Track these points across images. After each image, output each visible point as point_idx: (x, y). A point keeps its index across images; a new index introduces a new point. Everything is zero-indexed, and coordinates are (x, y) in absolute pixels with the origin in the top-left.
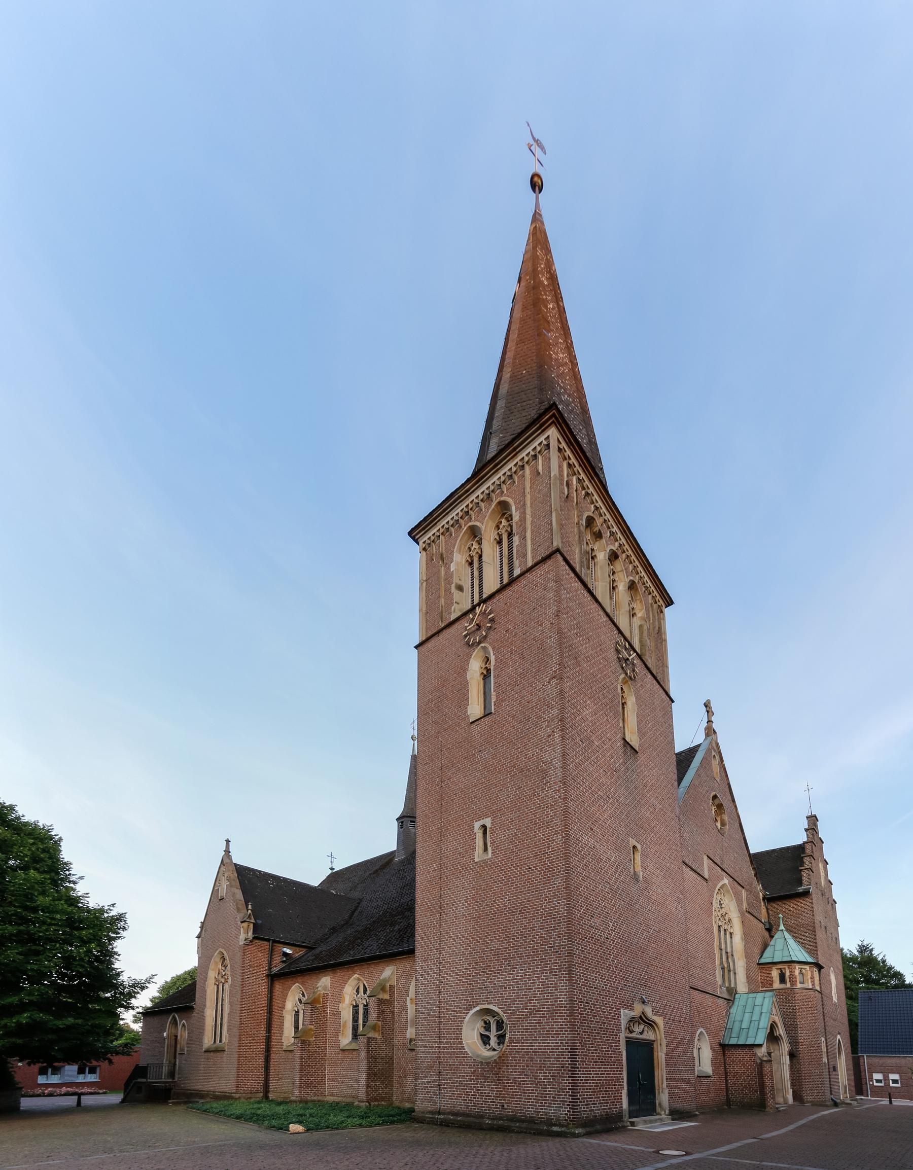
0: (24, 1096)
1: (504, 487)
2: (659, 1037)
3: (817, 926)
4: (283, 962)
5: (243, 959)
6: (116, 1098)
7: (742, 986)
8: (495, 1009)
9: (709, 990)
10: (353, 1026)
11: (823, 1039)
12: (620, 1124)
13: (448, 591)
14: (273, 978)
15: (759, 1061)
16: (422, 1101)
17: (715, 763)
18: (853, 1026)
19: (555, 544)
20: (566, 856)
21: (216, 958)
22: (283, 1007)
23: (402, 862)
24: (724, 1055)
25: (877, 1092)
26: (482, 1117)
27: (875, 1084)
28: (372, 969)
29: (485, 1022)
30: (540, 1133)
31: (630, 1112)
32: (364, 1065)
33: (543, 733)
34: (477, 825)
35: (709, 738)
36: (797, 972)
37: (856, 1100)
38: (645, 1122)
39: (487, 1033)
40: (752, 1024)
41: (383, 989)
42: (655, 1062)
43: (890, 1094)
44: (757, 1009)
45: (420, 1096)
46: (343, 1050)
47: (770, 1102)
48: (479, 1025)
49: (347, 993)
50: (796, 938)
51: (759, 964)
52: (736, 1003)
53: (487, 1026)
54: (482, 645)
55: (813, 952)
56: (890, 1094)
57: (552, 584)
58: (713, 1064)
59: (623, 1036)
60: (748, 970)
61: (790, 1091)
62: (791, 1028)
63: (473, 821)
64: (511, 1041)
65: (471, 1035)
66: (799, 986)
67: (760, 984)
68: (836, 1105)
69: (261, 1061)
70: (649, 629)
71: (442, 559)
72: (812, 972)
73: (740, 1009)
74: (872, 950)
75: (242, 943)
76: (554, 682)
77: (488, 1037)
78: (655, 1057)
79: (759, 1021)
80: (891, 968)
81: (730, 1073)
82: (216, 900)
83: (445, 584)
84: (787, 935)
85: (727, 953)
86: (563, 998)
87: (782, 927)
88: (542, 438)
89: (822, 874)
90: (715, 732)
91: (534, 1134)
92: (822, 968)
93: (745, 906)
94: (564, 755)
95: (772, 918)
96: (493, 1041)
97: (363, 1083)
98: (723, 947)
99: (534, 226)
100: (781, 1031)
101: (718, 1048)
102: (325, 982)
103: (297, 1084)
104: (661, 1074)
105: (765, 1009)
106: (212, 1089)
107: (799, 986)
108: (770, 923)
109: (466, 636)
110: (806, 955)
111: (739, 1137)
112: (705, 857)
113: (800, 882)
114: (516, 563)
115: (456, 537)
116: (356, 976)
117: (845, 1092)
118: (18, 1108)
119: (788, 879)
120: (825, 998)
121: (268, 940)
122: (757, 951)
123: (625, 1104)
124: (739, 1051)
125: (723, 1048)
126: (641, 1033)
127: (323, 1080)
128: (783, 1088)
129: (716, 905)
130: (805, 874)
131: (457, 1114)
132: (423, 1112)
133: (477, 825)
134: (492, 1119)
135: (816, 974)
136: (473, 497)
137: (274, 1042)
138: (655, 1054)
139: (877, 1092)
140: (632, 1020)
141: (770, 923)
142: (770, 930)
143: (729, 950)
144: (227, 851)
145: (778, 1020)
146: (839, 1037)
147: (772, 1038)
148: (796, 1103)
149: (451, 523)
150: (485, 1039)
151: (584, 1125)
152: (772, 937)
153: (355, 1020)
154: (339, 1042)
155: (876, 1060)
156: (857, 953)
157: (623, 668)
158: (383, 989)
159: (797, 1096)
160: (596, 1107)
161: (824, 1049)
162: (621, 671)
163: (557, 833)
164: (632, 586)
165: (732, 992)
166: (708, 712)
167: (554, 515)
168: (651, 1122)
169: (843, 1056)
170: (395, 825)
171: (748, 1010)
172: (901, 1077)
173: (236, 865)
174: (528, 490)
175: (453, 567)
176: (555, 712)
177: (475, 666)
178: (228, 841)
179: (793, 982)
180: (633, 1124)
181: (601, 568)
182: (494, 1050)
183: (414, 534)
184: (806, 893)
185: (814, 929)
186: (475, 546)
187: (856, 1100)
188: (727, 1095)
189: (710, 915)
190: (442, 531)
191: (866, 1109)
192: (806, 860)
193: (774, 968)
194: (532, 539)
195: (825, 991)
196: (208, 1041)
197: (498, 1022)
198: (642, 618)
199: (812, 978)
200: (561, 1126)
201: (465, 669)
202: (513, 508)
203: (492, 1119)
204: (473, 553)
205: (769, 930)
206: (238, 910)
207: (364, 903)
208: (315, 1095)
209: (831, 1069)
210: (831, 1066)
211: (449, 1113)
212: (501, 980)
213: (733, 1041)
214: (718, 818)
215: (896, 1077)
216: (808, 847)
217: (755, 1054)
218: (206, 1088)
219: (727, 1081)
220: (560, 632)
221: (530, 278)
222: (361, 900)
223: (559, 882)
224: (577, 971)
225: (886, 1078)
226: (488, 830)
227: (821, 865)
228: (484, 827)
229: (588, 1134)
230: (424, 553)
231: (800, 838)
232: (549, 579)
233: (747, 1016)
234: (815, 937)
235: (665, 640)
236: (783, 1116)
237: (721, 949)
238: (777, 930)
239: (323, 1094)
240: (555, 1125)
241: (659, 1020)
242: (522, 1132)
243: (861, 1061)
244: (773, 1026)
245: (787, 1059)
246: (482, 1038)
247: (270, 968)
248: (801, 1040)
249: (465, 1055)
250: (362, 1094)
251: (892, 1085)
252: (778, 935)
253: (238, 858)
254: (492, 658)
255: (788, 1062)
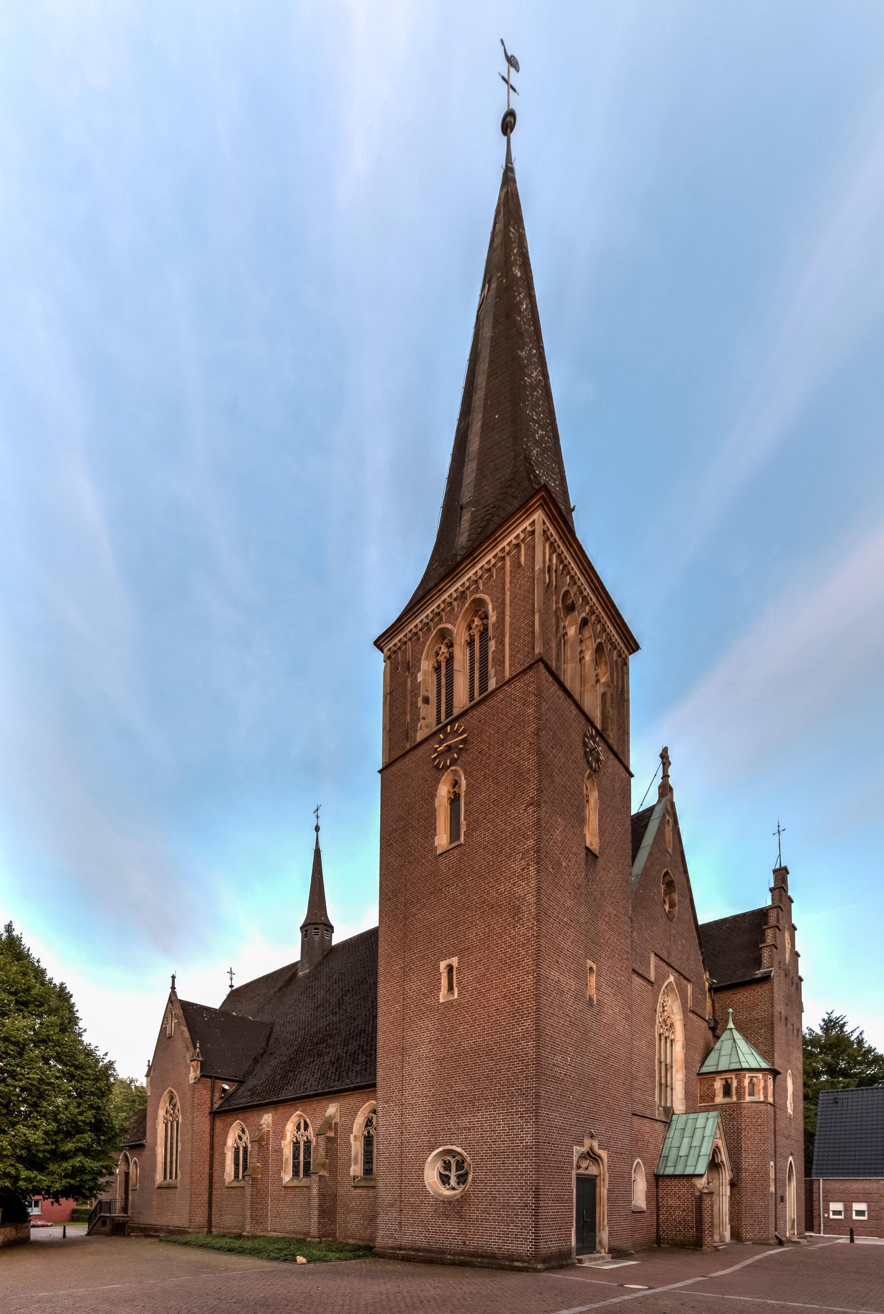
0: (34, 1226)
1: (481, 582)
2: (602, 1171)
3: (776, 1019)
4: (221, 1098)
5: (193, 1097)
6: (78, 1231)
7: (679, 1105)
8: (459, 1149)
9: (648, 1113)
10: (294, 1163)
11: (772, 1163)
12: (570, 1261)
13: (414, 705)
14: (215, 1114)
15: (697, 1194)
16: (383, 1237)
17: (668, 829)
18: (809, 1137)
19: (537, 651)
20: (537, 997)
21: (165, 1097)
22: (225, 1144)
23: (307, 976)
24: (657, 1187)
25: (833, 1227)
26: (443, 1253)
27: (832, 1217)
28: (314, 1106)
29: (445, 1162)
30: (502, 1268)
31: (577, 1249)
32: (315, 1202)
33: (516, 866)
34: (443, 965)
35: (664, 800)
36: (746, 1082)
37: (805, 1237)
38: (590, 1260)
39: (447, 1173)
40: (692, 1151)
41: (330, 1127)
42: (598, 1198)
43: (852, 1230)
44: (698, 1133)
45: (381, 1233)
46: (286, 1187)
47: (707, 1240)
48: (439, 1164)
49: (289, 1130)
50: (747, 1038)
51: (699, 1074)
52: (673, 1126)
53: (447, 1166)
54: (453, 768)
55: (767, 1054)
56: (852, 1230)
57: (532, 698)
58: (648, 1198)
59: (574, 1172)
60: (687, 1083)
61: (728, 1227)
62: (735, 1151)
63: (438, 960)
64: (474, 1181)
65: (431, 1175)
66: (748, 1098)
67: (699, 1100)
68: (781, 1243)
69: (206, 1198)
70: (612, 695)
71: (408, 668)
72: (765, 1081)
73: (678, 1132)
74: (843, 1025)
75: (191, 1082)
76: (531, 809)
77: (448, 1177)
78: (598, 1193)
79: (700, 1147)
80: (870, 1050)
81: (663, 1206)
82: (164, 1040)
83: (412, 697)
84: (737, 1035)
85: (666, 1065)
86: (529, 1140)
87: (731, 1025)
88: (526, 524)
89: (788, 946)
90: (671, 789)
91: (496, 1268)
92: (779, 1073)
93: (690, 1004)
94: (539, 889)
95: (718, 1013)
96: (453, 1181)
97: (315, 1220)
98: (663, 1059)
99: (505, 190)
100: (724, 1157)
101: (653, 1181)
102: (267, 1119)
103: (248, 1220)
104: (603, 1210)
105: (708, 1132)
106: (166, 1224)
107: (748, 1098)
108: (715, 1020)
109: (435, 758)
110: (759, 1059)
111: (683, 1279)
112: (652, 956)
113: (758, 963)
114: (492, 672)
115: (425, 642)
116: (298, 1112)
117: (793, 1228)
118: (28, 1237)
119: (746, 959)
120: (778, 1112)
121: (210, 1077)
122: (698, 1058)
123: (573, 1243)
124: (675, 1182)
125: (657, 1180)
126: (587, 1169)
127: (266, 1216)
128: (721, 1223)
129: (659, 1009)
130: (766, 953)
131: (417, 1250)
132: (384, 1248)
133: (443, 965)
134: (454, 1255)
135: (770, 1082)
136: (445, 596)
137: (215, 1179)
138: (598, 1189)
139: (833, 1227)
140: (583, 1157)
141: (715, 1020)
142: (716, 1029)
143: (668, 1062)
144: (173, 988)
145: (720, 1143)
146: (791, 1158)
147: (714, 1165)
148: (734, 1241)
149: (420, 626)
150: (444, 1179)
151: (544, 1261)
152: (717, 1037)
153: (296, 1156)
154: (281, 1179)
155: (835, 1185)
156: (820, 1032)
157: (588, 762)
158: (330, 1127)
159: (736, 1235)
160: (550, 1245)
161: (772, 1176)
162: (586, 766)
163: (528, 973)
164: (599, 649)
165: (669, 1112)
166: (664, 764)
167: (537, 617)
168: (595, 1259)
169: (794, 1183)
170: (299, 935)
171: (688, 1133)
172: (869, 1207)
173: (180, 1001)
174: (508, 586)
175: (420, 678)
176: (531, 843)
177: (443, 791)
178: (173, 977)
179: (740, 1095)
180: (580, 1261)
181: (571, 646)
182: (454, 1189)
183: (379, 643)
184: (766, 978)
185: (772, 1024)
186: (444, 649)
187: (805, 1237)
188: (658, 1232)
189: (653, 1026)
190: (409, 635)
191: (820, 1248)
192: (769, 933)
193: (718, 1078)
194: (511, 644)
195: (779, 1102)
196: (159, 1178)
197: (458, 1161)
198: (607, 684)
199: (765, 1088)
200: (523, 1261)
201: (432, 795)
202: (490, 607)
203: (454, 1255)
204: (441, 658)
205: (713, 1029)
206: (188, 1049)
207: (277, 1029)
208: (262, 1231)
209: (779, 1199)
210: (779, 1196)
211: (410, 1249)
212: (465, 1122)
213: (669, 1171)
214: (667, 899)
215: (862, 1207)
216: (773, 914)
217: (693, 1186)
218: (159, 1223)
219: (658, 1216)
220: (540, 753)
221: (502, 276)
222: (272, 1025)
223: (528, 1023)
224: (543, 1112)
225: (848, 1209)
226: (455, 970)
227: (787, 935)
228: (450, 968)
229: (547, 1270)
230: (388, 662)
231: (766, 901)
232: (529, 692)
233: (686, 1141)
234: (773, 1034)
235: (628, 700)
236: (723, 1256)
237: (660, 1062)
238: (725, 1029)
239: (266, 1230)
240: (517, 1261)
241: (603, 1154)
242: (484, 1267)
243: (815, 1186)
244: (716, 1151)
245: (727, 1190)
246: (441, 1178)
247: (212, 1105)
248: (744, 1165)
249: (427, 1195)
250: (314, 1230)
251: (855, 1217)
252: (726, 1035)
253: (181, 996)
254: (464, 782)
255: (728, 1193)
